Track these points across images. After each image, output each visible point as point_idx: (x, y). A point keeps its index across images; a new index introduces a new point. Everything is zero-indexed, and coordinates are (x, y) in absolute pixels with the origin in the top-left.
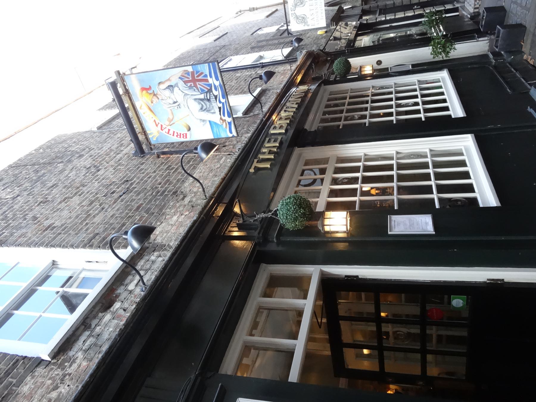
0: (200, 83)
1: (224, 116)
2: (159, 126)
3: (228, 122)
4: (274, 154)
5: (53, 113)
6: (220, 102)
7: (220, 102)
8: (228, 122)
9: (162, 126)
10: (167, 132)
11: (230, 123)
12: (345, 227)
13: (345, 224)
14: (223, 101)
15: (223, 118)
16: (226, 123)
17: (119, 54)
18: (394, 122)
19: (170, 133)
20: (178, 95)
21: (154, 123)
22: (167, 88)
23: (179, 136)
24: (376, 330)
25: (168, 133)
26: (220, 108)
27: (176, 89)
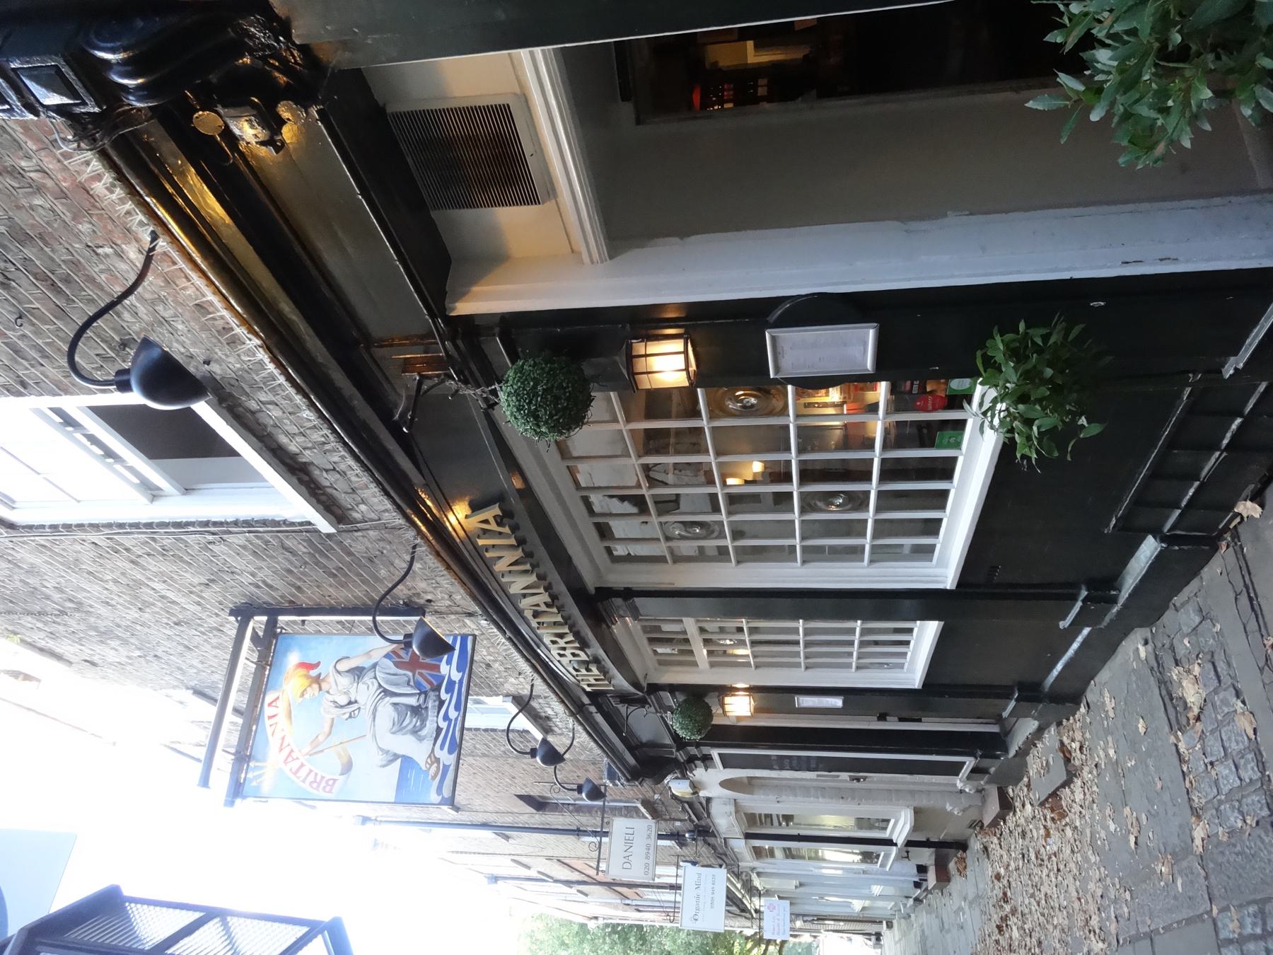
0: (424, 672)
1: (442, 748)
2: (286, 751)
3: (444, 765)
4: (497, 505)
5: (20, 461)
6: (446, 717)
7: (446, 717)
8: (444, 765)
9: (292, 751)
10: (294, 771)
11: (446, 768)
12: (684, 373)
13: (683, 367)
14: (453, 714)
15: (438, 753)
16: (438, 768)
17: (341, 817)
18: (995, 330)
19: (298, 775)
20: (365, 692)
21: (280, 741)
22: (348, 671)
23: (315, 785)
24: (749, 62)
25: (295, 773)
26: (439, 730)
27: (367, 679)
